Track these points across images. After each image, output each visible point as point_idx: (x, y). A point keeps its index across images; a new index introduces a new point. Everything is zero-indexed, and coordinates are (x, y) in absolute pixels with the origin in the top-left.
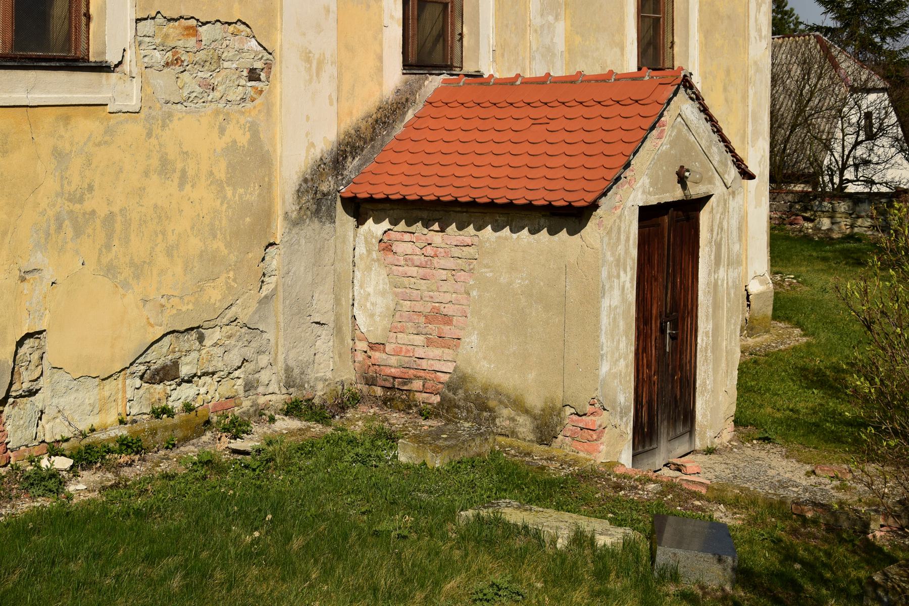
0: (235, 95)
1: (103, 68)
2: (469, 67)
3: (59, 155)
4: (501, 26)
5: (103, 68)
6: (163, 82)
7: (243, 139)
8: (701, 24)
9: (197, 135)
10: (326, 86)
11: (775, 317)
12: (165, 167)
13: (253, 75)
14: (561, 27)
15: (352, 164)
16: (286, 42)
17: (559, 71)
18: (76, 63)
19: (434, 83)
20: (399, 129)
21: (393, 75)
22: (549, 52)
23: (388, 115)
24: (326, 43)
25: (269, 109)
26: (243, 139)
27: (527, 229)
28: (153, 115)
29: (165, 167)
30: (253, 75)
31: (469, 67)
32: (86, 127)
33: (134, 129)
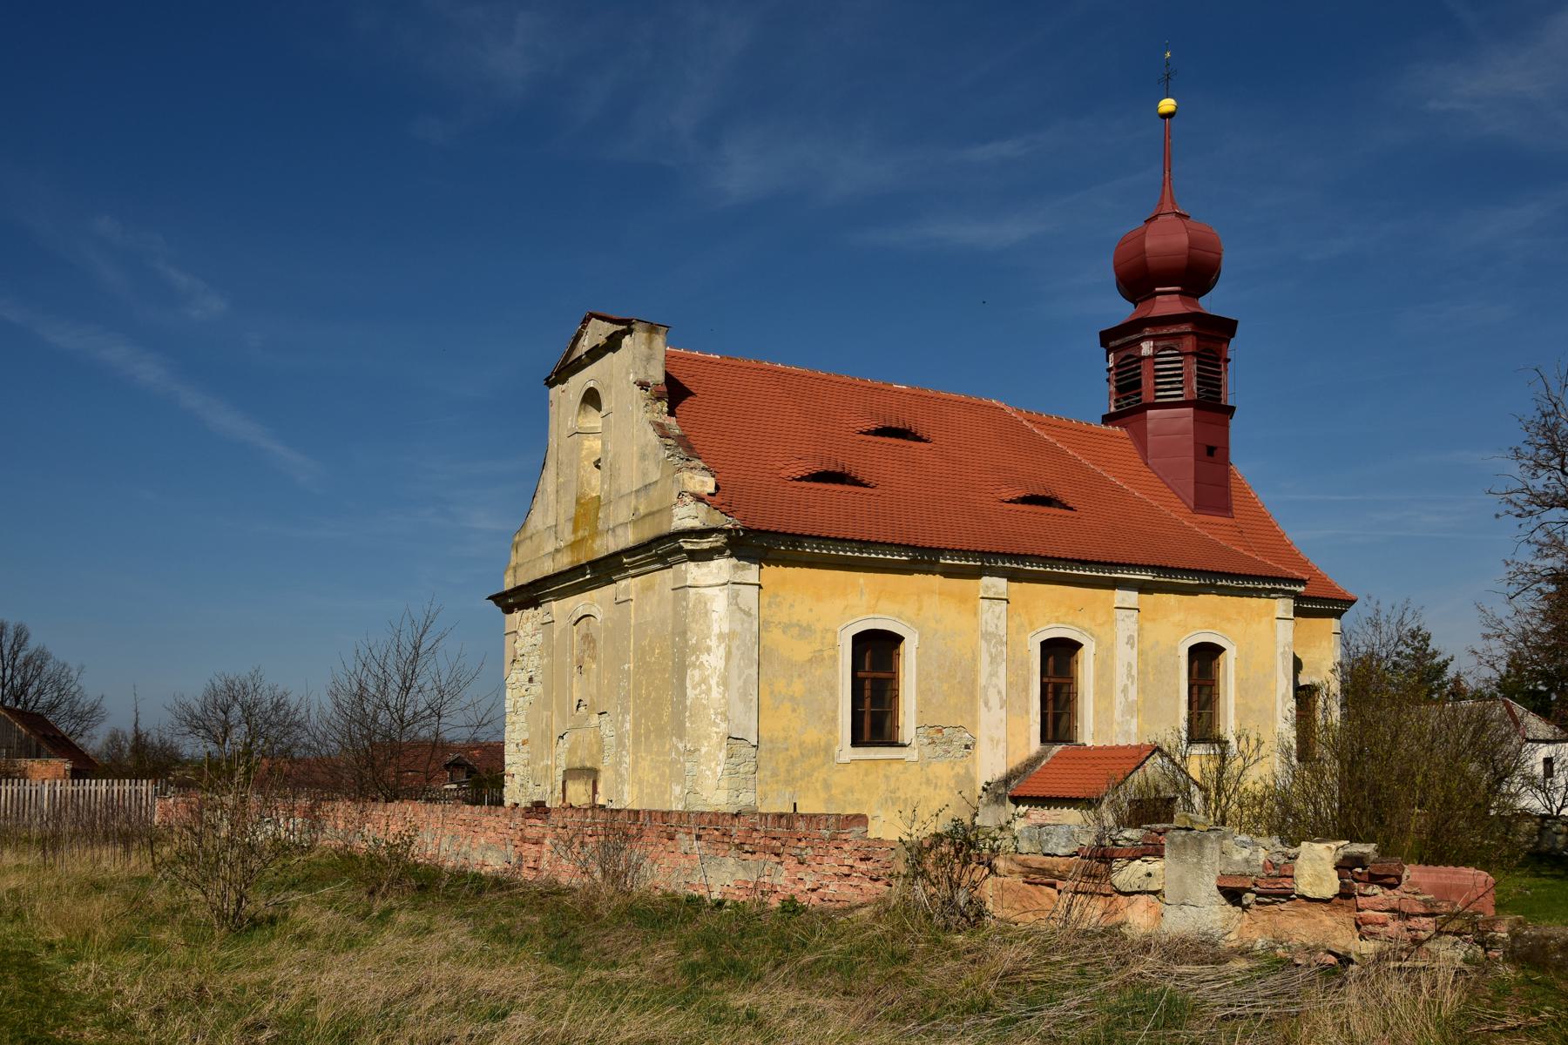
0: (959, 754)
1: (903, 746)
2: (1080, 741)
3: (886, 777)
4: (1097, 721)
5: (903, 746)
6: (927, 750)
7: (962, 772)
8: (1236, 716)
9: (942, 770)
10: (1001, 751)
11: (1191, 741)
12: (928, 782)
13: (967, 747)
14: (1134, 721)
15: (1014, 783)
16: (982, 734)
17: (1134, 743)
18: (894, 744)
19: (1057, 749)
20: (1038, 768)
21: (1035, 745)
22: (1127, 733)
23: (1032, 763)
24: (1001, 734)
25: (974, 760)
26: (962, 772)
27: (632, 366)
28: (924, 763)
29: (928, 782)
30: (967, 747)
31: (1080, 741)
32: (896, 767)
33: (916, 768)
